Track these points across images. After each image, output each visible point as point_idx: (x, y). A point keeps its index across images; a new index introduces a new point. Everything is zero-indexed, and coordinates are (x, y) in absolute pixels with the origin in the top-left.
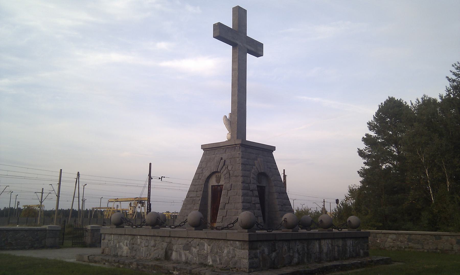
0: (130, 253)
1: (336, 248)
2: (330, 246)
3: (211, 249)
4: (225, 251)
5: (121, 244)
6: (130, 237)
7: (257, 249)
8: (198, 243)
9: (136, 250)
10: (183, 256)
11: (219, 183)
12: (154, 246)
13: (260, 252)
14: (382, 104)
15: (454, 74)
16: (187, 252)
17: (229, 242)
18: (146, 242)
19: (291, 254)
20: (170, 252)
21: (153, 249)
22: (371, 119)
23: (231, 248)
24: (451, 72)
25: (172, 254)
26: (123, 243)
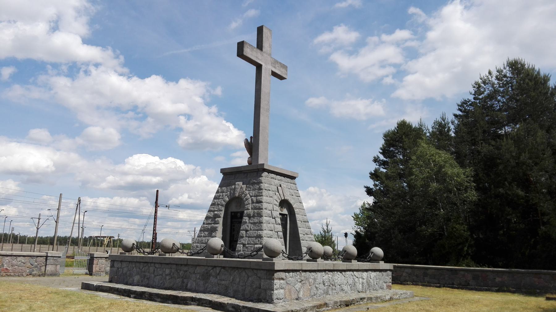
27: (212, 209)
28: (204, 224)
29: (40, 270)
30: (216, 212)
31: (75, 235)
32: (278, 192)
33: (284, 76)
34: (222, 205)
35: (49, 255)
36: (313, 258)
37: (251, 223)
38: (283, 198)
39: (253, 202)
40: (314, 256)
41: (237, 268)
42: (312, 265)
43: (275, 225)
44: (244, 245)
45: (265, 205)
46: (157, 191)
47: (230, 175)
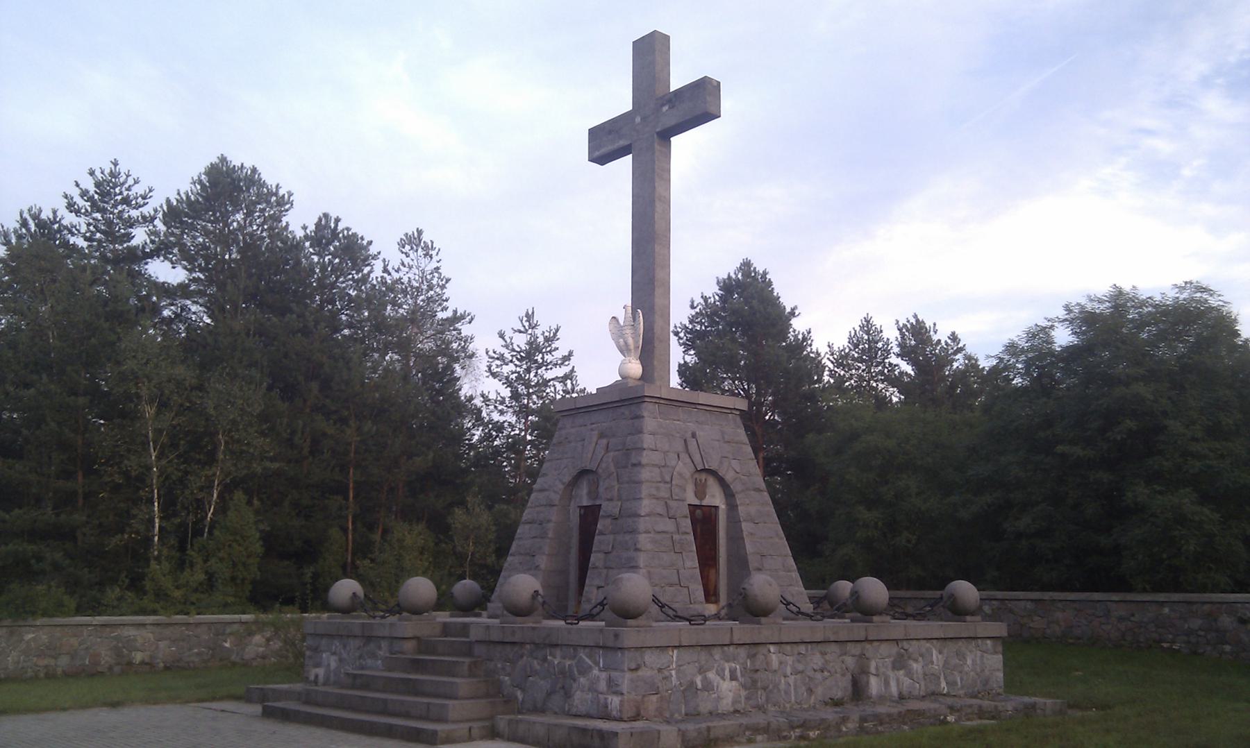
0: (748, 698)
6: (742, 652)
9: (765, 689)
10: (893, 684)
11: (701, 499)
15: (84, 194)
16: (902, 672)
18: (799, 661)
21: (819, 676)
24: (77, 185)
25: (868, 682)
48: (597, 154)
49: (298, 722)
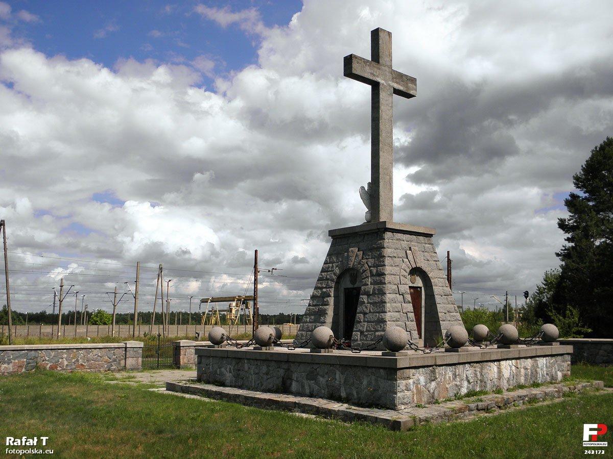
1: (522, 370)
2: (514, 368)
3: (345, 379)
4: (365, 382)
5: (223, 369)
6: (234, 362)
7: (409, 378)
8: (326, 371)
9: (242, 379)
10: (307, 387)
12: (267, 374)
13: (414, 383)
14: (596, 148)
17: (370, 370)
19: (458, 383)
20: (288, 382)
21: (265, 377)
22: (579, 171)
23: (373, 378)
25: (291, 384)
26: (226, 369)
27: (320, 285)
28: (309, 305)
29: (119, 364)
30: (324, 290)
31: (159, 310)
32: (407, 258)
33: (412, 92)
34: (332, 280)
35: (128, 346)
36: (453, 347)
37: (371, 303)
38: (414, 266)
39: (372, 275)
40: (454, 345)
41: (350, 366)
42: (453, 357)
43: (403, 304)
44: (362, 333)
45: (388, 278)
46: (256, 251)
47: (341, 238)
48: (381, 34)
49: (378, 102)
